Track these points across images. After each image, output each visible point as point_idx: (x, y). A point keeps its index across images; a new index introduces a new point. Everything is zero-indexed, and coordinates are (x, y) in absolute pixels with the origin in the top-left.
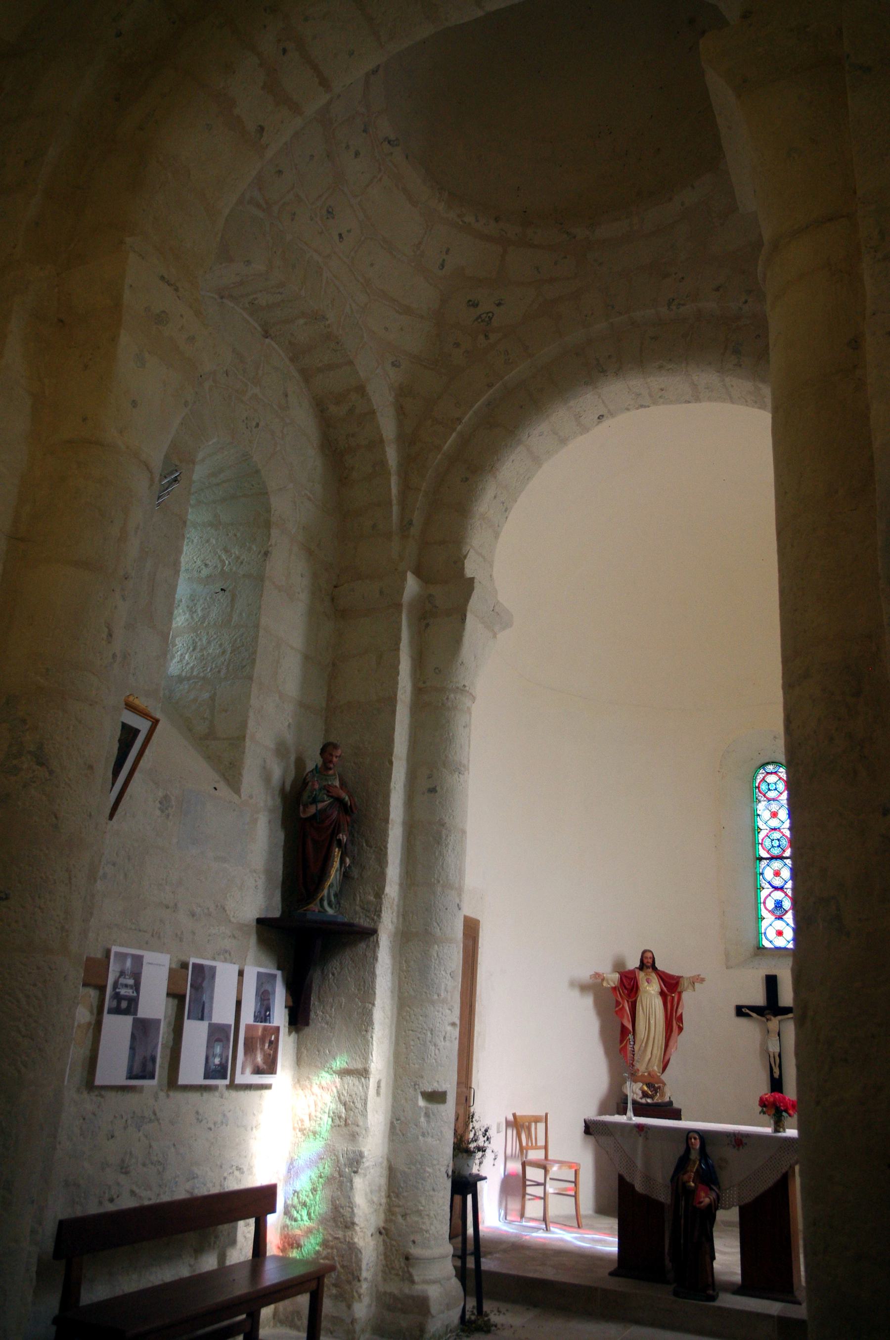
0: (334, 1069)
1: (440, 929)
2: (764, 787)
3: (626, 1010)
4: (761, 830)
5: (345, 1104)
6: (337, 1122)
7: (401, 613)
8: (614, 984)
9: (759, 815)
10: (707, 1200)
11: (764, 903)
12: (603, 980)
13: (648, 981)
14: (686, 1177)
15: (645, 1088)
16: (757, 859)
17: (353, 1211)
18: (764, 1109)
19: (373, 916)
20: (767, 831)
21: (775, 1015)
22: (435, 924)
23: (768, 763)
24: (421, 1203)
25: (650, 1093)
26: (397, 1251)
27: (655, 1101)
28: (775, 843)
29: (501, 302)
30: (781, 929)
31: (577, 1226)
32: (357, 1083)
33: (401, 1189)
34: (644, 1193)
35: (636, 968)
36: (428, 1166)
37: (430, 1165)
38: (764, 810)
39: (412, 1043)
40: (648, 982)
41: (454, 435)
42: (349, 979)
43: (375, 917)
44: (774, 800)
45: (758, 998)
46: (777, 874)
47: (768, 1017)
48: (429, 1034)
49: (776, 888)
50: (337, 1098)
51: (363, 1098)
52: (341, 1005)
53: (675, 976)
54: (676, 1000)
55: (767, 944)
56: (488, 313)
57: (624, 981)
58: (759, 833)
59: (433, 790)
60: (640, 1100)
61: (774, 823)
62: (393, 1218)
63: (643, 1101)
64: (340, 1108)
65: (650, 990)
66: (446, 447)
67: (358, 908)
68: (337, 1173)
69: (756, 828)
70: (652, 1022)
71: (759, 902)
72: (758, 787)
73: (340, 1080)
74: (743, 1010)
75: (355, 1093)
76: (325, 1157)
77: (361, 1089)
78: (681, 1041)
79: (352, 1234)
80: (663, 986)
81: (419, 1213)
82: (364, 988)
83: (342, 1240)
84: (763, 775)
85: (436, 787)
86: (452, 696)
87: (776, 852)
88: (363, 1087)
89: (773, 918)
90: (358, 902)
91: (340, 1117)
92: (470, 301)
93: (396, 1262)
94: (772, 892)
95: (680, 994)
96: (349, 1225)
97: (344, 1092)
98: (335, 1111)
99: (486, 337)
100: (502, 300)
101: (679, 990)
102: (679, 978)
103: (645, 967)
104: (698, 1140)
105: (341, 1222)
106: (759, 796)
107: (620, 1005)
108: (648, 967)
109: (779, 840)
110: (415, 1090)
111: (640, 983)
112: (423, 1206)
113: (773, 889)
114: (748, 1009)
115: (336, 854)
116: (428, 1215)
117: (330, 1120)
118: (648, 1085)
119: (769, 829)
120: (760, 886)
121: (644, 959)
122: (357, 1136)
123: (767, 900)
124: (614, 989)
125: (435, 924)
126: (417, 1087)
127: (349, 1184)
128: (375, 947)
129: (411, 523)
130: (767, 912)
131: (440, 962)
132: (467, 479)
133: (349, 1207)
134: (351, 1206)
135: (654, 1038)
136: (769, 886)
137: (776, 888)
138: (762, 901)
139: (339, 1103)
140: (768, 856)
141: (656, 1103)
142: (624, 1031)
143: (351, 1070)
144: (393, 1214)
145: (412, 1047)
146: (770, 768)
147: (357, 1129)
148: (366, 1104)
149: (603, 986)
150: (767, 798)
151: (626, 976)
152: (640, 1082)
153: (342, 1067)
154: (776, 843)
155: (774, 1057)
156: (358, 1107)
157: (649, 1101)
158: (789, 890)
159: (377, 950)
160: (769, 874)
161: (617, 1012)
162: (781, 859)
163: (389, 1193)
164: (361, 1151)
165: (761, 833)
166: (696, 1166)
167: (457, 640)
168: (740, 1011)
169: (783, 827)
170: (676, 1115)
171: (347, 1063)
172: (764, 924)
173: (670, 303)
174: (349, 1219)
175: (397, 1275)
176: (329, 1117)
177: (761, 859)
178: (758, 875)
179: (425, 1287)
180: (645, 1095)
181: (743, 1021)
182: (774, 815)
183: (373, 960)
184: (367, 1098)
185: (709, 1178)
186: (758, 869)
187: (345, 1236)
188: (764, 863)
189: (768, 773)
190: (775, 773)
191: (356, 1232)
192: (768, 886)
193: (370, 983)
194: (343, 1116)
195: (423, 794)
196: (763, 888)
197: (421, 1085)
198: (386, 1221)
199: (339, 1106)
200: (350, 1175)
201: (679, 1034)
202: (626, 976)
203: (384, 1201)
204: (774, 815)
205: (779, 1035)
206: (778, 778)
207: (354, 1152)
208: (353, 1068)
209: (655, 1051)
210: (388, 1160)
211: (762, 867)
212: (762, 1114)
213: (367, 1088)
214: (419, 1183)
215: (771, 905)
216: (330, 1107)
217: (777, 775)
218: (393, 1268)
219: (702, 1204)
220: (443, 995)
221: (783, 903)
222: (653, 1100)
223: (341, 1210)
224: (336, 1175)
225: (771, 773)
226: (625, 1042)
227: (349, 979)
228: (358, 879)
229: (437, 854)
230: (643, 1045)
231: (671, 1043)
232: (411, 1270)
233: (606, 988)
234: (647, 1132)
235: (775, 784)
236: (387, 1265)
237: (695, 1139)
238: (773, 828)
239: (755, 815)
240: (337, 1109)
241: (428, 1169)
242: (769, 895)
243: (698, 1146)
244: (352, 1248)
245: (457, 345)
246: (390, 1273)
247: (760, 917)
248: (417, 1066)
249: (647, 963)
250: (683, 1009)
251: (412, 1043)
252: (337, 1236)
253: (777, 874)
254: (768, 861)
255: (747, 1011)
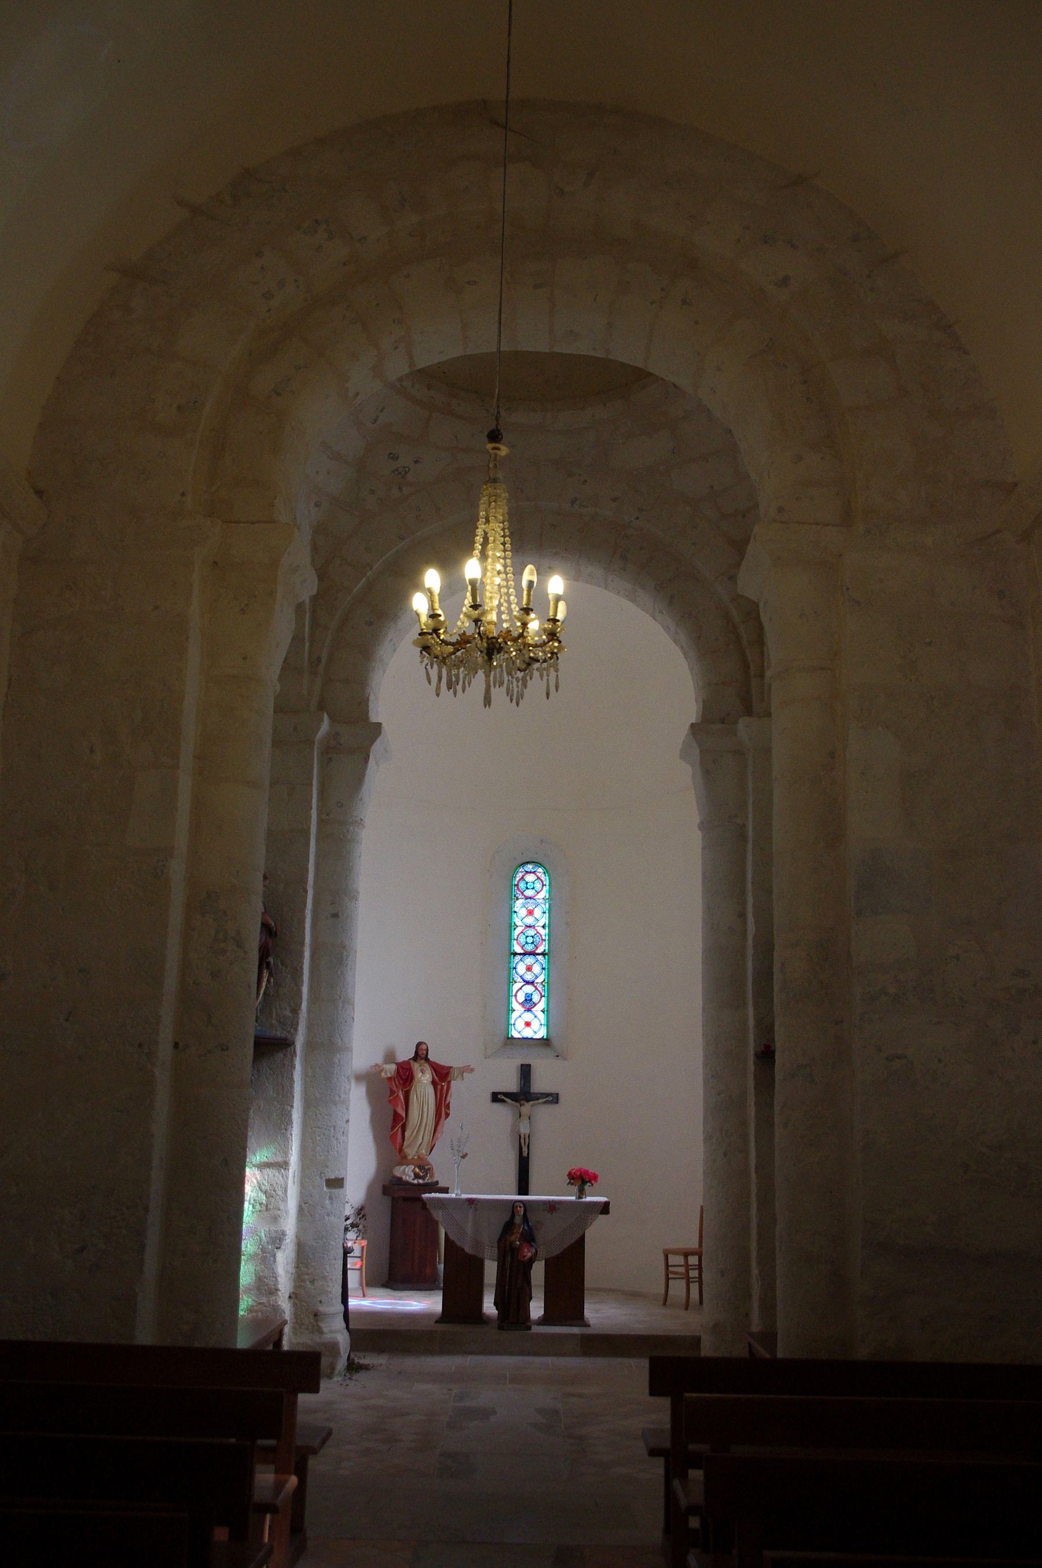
0: (253, 1163)
1: (341, 1040)
2: (522, 885)
3: (400, 1099)
4: (517, 926)
5: (265, 1193)
6: (258, 1207)
7: (313, 750)
8: (391, 1074)
9: (515, 912)
10: (530, 1254)
11: (516, 996)
12: (382, 1071)
13: (422, 1071)
14: (513, 1238)
15: (417, 1170)
16: (512, 954)
17: (276, 1280)
18: (572, 1181)
19: (289, 1028)
20: (523, 928)
21: (528, 1101)
22: (337, 1035)
23: (528, 863)
24: (326, 1270)
25: (422, 1174)
26: (307, 1310)
27: (426, 1181)
28: (530, 940)
29: (419, 460)
30: (530, 1021)
31: (362, 1296)
32: (277, 1174)
33: (309, 1260)
34: (473, 1253)
35: (410, 1059)
36: (332, 1240)
37: (333, 1239)
38: (521, 907)
39: (318, 1138)
40: (422, 1072)
41: (364, 579)
42: (267, 1085)
43: (292, 1030)
44: (530, 898)
45: (512, 1085)
46: (529, 969)
47: (522, 1102)
48: (332, 1129)
49: (527, 983)
50: (258, 1188)
51: (283, 1186)
52: (260, 1108)
53: (445, 1066)
54: (445, 1087)
55: (516, 1035)
56: (404, 467)
57: (401, 1071)
58: (515, 929)
59: (335, 916)
60: (413, 1181)
61: (529, 920)
62: (303, 1284)
63: (416, 1182)
64: (261, 1196)
65: (424, 1078)
66: (354, 591)
67: (274, 1022)
68: (260, 1250)
69: (513, 925)
70: (425, 1110)
71: (511, 995)
72: (517, 885)
73: (259, 1172)
74: (499, 1096)
75: (275, 1182)
76: (247, 1237)
77: (282, 1180)
78: (447, 1124)
79: (276, 1299)
80: (435, 1076)
81: (324, 1278)
82: (283, 1091)
83: (267, 1304)
84: (523, 874)
85: (338, 912)
86: (351, 828)
87: (530, 948)
88: (283, 1176)
89: (523, 1009)
90: (274, 1015)
91: (261, 1204)
92: (391, 454)
93: (306, 1318)
94: (523, 986)
95: (449, 1082)
96: (273, 1291)
97: (264, 1182)
98: (257, 1199)
99: (400, 488)
100: (420, 458)
101: (449, 1079)
102: (451, 1068)
103: (419, 1058)
104: (523, 1208)
105: (265, 1290)
106: (517, 894)
107: (395, 1093)
108: (422, 1059)
109: (533, 937)
110: (321, 1178)
111: (415, 1073)
112: (327, 1273)
113: (525, 983)
114: (504, 1096)
115: (265, 974)
116: (331, 1280)
117: (251, 1206)
118: (419, 1167)
119: (524, 926)
120: (513, 980)
121: (419, 1051)
122: (278, 1218)
123: (519, 993)
124: (389, 1079)
125: (337, 1035)
126: (323, 1175)
127: (272, 1258)
128: (292, 1056)
129: (319, 659)
130: (518, 1004)
131: (341, 1068)
132: (371, 624)
133: (273, 1277)
134: (275, 1276)
135: (426, 1124)
136: (521, 980)
137: (527, 983)
138: (514, 994)
139: (260, 1192)
140: (522, 952)
141: (426, 1183)
142: (396, 1117)
143: (271, 1163)
144: (303, 1281)
145: (318, 1142)
146: (529, 867)
147: (279, 1212)
148: (286, 1191)
149: (381, 1075)
150: (525, 896)
151: (402, 1068)
152: (411, 1164)
153: (262, 1161)
154: (530, 940)
155: (525, 1138)
156: (279, 1194)
157: (421, 1181)
158: (539, 984)
159: (295, 1058)
160: (521, 968)
161: (390, 1101)
162: (534, 955)
163: (298, 1264)
164: (283, 1230)
165: (517, 929)
166: (522, 1228)
167: (359, 779)
168: (496, 1097)
169: (537, 925)
170: (446, 1190)
171: (267, 1157)
172: (514, 1016)
173: (573, 502)
174: (273, 1287)
175: (307, 1329)
176: (250, 1204)
177: (515, 954)
178: (512, 969)
179: (333, 1335)
180: (417, 1176)
181: (497, 1106)
182: (530, 913)
183: (291, 1068)
184: (287, 1186)
185: (529, 1238)
186: (512, 963)
187: (269, 1302)
188: (518, 958)
189: (527, 872)
190: (534, 873)
191: (279, 1298)
192: (519, 979)
193: (289, 1088)
194: (264, 1202)
195: (327, 918)
196: (516, 982)
197: (326, 1173)
198: (295, 1287)
199: (259, 1194)
200: (273, 1251)
201: (445, 1119)
202: (402, 1068)
203: (294, 1271)
204: (530, 913)
205: (529, 1119)
206: (536, 878)
207: (276, 1232)
208: (273, 1162)
209: (425, 1138)
210: (297, 1237)
211: (516, 962)
212: (570, 1185)
213: (287, 1178)
214: (325, 1254)
215: (521, 997)
216: (251, 1195)
217: (536, 874)
218: (302, 1324)
219: (526, 1258)
220: (343, 1096)
221: (533, 997)
222: (424, 1180)
223: (265, 1280)
224: (259, 1251)
225: (530, 872)
226: (396, 1129)
227: (267, 1085)
228: (273, 995)
229: (339, 973)
230: (415, 1131)
231: (439, 1127)
232: (320, 1324)
233: (384, 1079)
234: (476, 1205)
235: (533, 883)
236: (297, 1323)
237: (520, 1207)
238: (528, 925)
239: (511, 912)
240: (258, 1197)
241: (332, 1243)
242: (521, 988)
243: (522, 1213)
244: (276, 1309)
245: (372, 492)
246: (300, 1328)
247: (511, 1009)
248: (323, 1157)
249: (421, 1054)
250: (451, 1098)
251: (318, 1138)
252: (262, 1301)
253: (529, 969)
254: (522, 956)
255: (503, 1097)
